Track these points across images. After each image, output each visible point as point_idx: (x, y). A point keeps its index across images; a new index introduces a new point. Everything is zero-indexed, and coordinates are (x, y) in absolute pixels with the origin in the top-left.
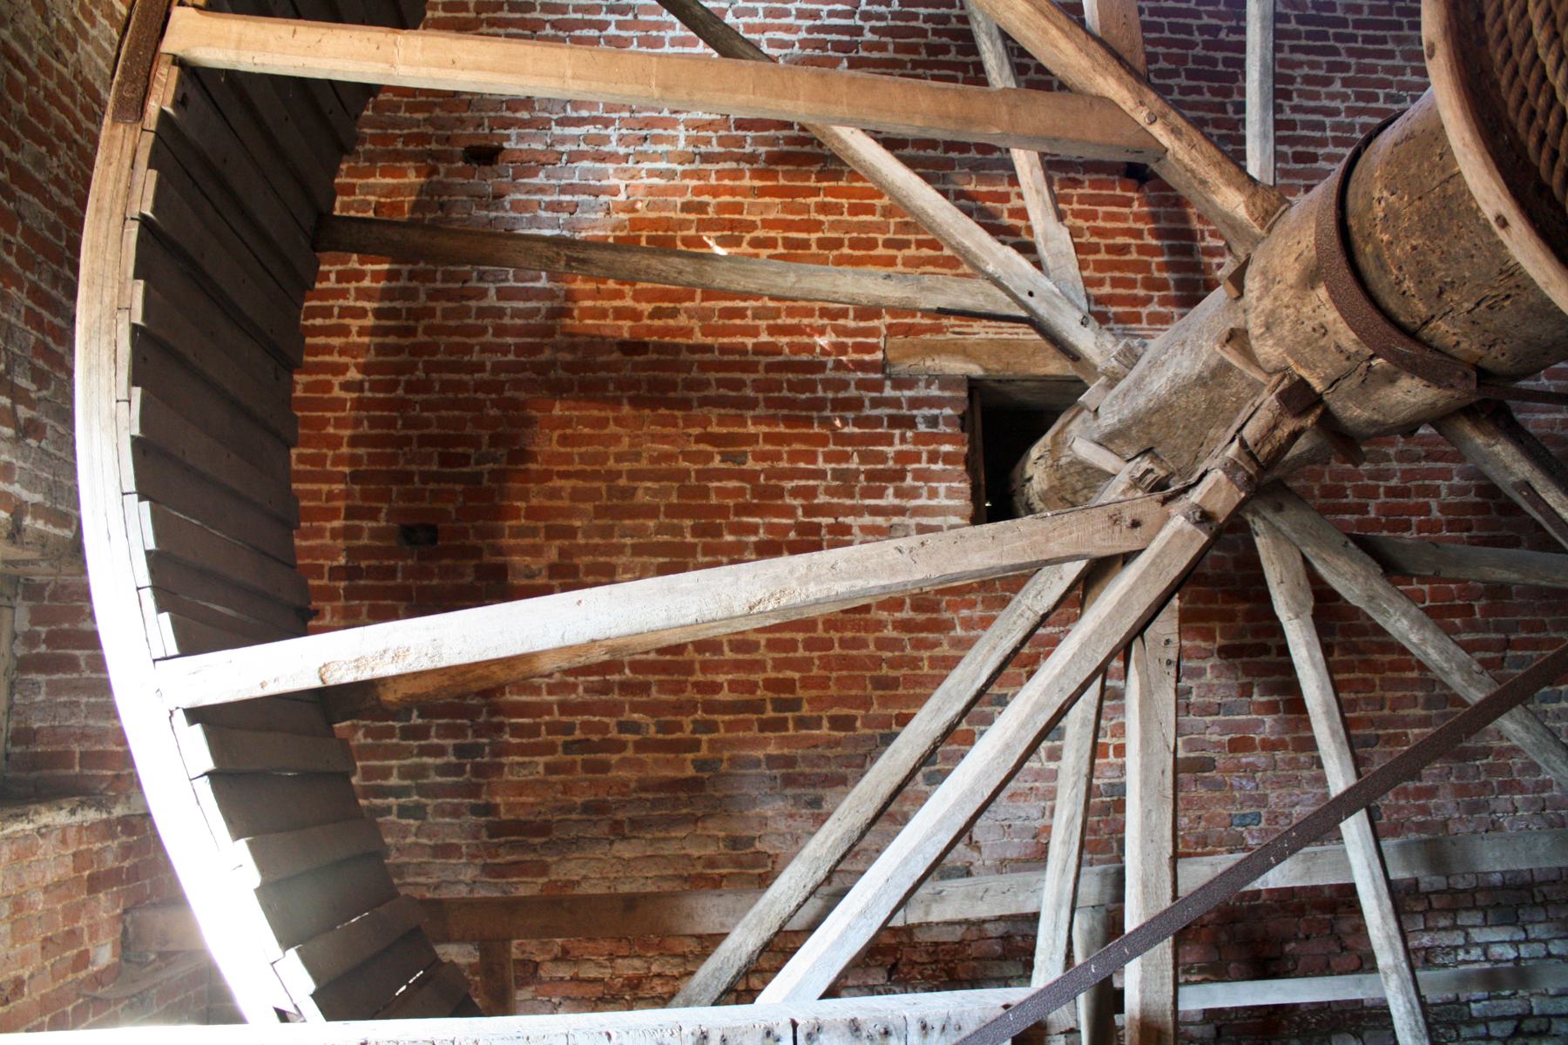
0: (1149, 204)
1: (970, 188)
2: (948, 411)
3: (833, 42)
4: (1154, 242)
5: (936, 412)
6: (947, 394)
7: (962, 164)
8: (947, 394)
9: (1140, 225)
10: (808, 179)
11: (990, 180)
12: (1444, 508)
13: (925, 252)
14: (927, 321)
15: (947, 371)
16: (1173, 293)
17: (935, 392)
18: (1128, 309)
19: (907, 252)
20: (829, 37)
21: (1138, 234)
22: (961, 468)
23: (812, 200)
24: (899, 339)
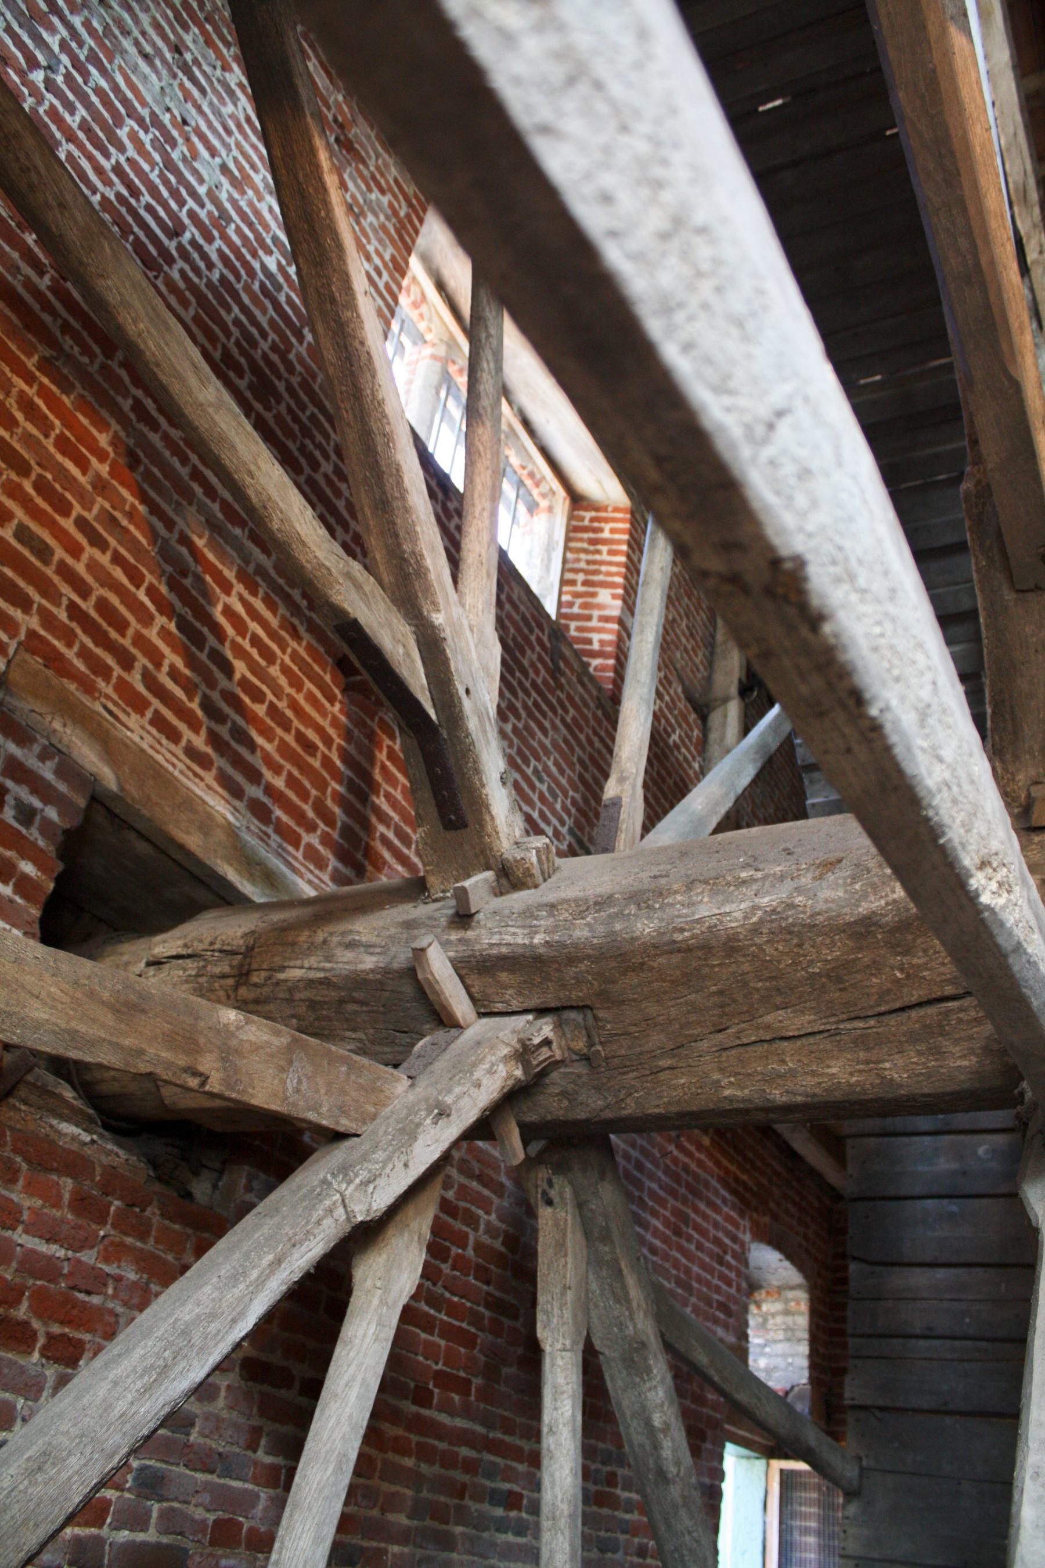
0: (348, 716)
1: (200, 543)
2: (52, 813)
3: (137, 238)
4: (338, 763)
5: (37, 803)
6: (62, 787)
7: (202, 509)
8: (62, 787)
9: (332, 732)
10: (29, 355)
11: (222, 555)
12: (479, 1247)
13: (118, 574)
14: (80, 665)
15: (75, 755)
16: (336, 835)
17: (47, 771)
18: (292, 823)
19: (96, 553)
20: (136, 229)
21: (328, 741)
22: (35, 912)
23: (20, 383)
24: (36, 662)
